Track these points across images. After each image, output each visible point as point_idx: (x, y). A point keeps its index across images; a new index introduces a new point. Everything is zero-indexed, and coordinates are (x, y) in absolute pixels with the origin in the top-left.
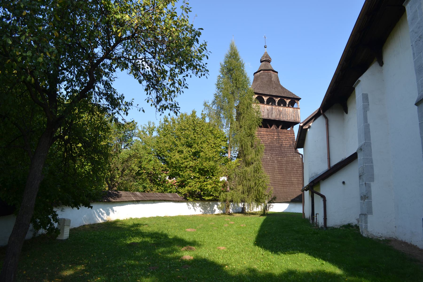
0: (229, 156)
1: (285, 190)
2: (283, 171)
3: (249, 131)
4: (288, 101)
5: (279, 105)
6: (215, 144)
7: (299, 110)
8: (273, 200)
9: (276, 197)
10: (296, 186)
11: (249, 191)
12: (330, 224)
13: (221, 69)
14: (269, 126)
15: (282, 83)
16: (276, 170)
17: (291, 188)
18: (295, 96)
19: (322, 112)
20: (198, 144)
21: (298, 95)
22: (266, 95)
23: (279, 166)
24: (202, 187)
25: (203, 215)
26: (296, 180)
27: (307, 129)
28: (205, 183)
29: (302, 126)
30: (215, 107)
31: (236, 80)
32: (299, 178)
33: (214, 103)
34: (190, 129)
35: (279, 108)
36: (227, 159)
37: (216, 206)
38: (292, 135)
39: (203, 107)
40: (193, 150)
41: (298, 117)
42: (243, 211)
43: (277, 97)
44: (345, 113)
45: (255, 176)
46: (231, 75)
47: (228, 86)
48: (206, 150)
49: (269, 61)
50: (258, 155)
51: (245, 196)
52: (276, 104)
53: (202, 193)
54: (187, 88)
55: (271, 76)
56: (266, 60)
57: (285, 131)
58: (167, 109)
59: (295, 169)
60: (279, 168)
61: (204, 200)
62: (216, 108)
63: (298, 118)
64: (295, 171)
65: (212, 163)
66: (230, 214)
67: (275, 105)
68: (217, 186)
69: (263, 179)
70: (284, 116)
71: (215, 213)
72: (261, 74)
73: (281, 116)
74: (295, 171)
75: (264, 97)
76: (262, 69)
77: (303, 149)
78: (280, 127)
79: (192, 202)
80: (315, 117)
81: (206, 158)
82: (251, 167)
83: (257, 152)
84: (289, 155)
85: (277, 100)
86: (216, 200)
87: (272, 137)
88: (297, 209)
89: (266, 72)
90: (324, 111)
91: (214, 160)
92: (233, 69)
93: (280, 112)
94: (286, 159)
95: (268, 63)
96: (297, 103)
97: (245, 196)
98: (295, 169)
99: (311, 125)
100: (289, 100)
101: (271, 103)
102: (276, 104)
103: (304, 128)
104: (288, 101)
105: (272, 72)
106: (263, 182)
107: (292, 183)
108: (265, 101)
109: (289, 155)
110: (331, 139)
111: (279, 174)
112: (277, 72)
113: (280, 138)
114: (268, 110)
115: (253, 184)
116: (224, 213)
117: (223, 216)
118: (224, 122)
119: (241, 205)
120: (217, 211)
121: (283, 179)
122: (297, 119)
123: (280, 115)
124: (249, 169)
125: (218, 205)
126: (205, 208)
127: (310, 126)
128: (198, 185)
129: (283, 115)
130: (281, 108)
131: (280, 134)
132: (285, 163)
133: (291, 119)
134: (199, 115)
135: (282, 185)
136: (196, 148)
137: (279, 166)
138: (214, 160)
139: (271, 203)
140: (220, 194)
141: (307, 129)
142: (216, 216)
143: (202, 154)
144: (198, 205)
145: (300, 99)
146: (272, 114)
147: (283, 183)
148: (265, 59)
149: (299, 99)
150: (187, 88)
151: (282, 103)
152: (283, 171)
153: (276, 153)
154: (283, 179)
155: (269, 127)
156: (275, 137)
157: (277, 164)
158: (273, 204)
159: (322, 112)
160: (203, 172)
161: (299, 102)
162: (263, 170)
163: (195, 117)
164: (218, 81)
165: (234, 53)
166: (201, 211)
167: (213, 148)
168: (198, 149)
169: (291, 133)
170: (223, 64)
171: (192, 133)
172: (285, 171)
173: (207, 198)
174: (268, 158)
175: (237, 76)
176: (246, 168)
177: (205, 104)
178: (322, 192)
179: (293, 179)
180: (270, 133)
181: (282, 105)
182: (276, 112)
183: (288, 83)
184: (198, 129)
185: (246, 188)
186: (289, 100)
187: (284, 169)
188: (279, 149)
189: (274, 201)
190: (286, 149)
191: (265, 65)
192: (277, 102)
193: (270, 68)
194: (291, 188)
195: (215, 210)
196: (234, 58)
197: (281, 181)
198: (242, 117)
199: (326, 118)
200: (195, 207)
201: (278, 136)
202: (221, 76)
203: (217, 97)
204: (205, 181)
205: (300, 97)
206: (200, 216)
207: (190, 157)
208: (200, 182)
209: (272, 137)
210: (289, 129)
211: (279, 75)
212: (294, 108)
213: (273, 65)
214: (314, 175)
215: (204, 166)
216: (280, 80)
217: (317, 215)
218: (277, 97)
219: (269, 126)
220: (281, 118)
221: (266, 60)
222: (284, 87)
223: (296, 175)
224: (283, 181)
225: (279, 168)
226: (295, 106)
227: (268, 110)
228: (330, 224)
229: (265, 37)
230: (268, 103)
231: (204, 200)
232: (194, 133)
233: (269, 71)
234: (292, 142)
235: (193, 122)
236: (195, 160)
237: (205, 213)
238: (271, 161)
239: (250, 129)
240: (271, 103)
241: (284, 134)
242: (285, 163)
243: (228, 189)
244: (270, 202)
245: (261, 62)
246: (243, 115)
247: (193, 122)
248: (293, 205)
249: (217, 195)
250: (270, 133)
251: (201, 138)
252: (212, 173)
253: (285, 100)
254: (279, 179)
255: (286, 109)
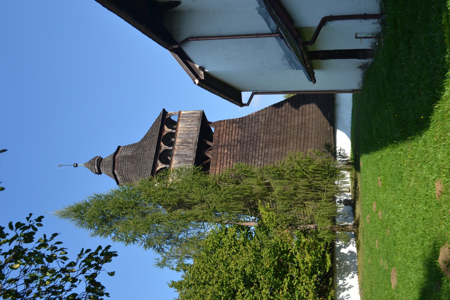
0: (253, 224)
1: (313, 136)
2: (282, 139)
3: (210, 187)
4: (167, 130)
5: (172, 144)
6: (230, 247)
7: (182, 112)
8: (331, 148)
9: (326, 145)
10: (307, 117)
11: (317, 189)
12: (374, 8)
13: (101, 235)
14: (207, 161)
15: (137, 139)
16: (281, 150)
17: (310, 126)
18: (158, 118)
19: (176, 46)
20: (230, 279)
21: (156, 114)
22: (155, 165)
23: (274, 145)
24: (309, 273)
25: (360, 272)
26: (296, 118)
27: (205, 73)
28: (301, 265)
29: (200, 80)
30: (167, 248)
31: (122, 208)
32: (293, 114)
33: (160, 250)
34: (202, 292)
35: (177, 144)
36: (259, 226)
37: (343, 250)
38: (222, 123)
39: (166, 268)
40: (241, 287)
41: (193, 113)
42: (351, 204)
43: (158, 147)
44: (180, 6)
45: (288, 177)
46: (113, 217)
47: (131, 222)
48: (241, 262)
49: (100, 160)
50: (253, 174)
51: (324, 196)
52: (171, 148)
53: (319, 272)
54: (40, 219)
55: (125, 157)
56: (97, 165)
57: (215, 136)
58: (97, 279)
59: (279, 120)
60: (278, 145)
61: (332, 269)
62: (170, 246)
63: (195, 113)
64: (283, 120)
65: (265, 252)
66: (357, 225)
67: (171, 150)
68: (307, 244)
69: (296, 164)
70: (192, 136)
71: (356, 252)
72: (119, 174)
73: (191, 140)
74: (283, 120)
75: (158, 169)
76: (111, 171)
77: (242, 93)
78: (209, 143)
79: (335, 292)
80: (185, 59)
81: (256, 262)
82: (273, 183)
83: (249, 174)
84: (256, 129)
85: (164, 147)
86: (332, 249)
87: (225, 156)
88: (345, 105)
89: (116, 165)
90: (176, 43)
91: (259, 248)
92: (103, 214)
93: (185, 142)
94: (262, 135)
95: (103, 161)
96: (171, 115)
97: (324, 196)
98: (279, 120)
99: (197, 66)
100: (166, 127)
101: (169, 158)
102: (171, 148)
103: (203, 78)
104: (167, 130)
105: (118, 155)
106: (299, 164)
107: (302, 124)
108: (164, 166)
109: (256, 129)
110: (222, 33)
111: (288, 146)
112: (119, 147)
113: (227, 143)
114: (180, 162)
115: (303, 182)
116: (356, 236)
117: (360, 237)
118: (193, 232)
119: (341, 208)
120: (352, 248)
121: (295, 140)
122: (196, 115)
123: (189, 143)
124: (277, 188)
125: (341, 247)
126: (347, 270)
127: (200, 67)
128: (305, 278)
129: (189, 138)
130: (178, 140)
131: (220, 144)
132: (268, 135)
133: (196, 125)
134: (178, 276)
135: (306, 141)
136: (238, 283)
137: (274, 145)
138: (259, 248)
139: (336, 153)
140: (321, 240)
141: (205, 73)
142: (360, 251)
143: (248, 270)
144: (341, 282)
145: (164, 110)
146: (186, 155)
147: (302, 138)
148: (96, 167)
149: (164, 112)
150: (40, 219)
151: (169, 140)
152: (282, 139)
153: (251, 149)
154: (295, 140)
155: (209, 160)
156: (226, 151)
157: (270, 149)
158: (338, 149)
159: (176, 46)
160: (281, 270)
161: (169, 112)
162: (278, 164)
163: (181, 283)
164: (122, 240)
165: (76, 211)
166: (353, 277)
167: (238, 251)
168: (239, 277)
169: (220, 126)
170: (93, 231)
171: (211, 288)
172: (282, 136)
173: (329, 263)
174: (259, 163)
175: (114, 206)
176: (275, 193)
177: (161, 265)
178: (314, 23)
179: (296, 124)
180: (219, 159)
181: (173, 139)
182: (183, 149)
183: (137, 129)
184: (204, 277)
185: (311, 195)
186: (166, 127)
187: (278, 137)
188: (245, 145)
189: (333, 147)
190: (246, 134)
191: (105, 167)
192: (167, 148)
193: (111, 159)
194: (310, 126)
195: (350, 252)
196: (85, 212)
197: (298, 141)
198: (187, 200)
199: (187, 40)
200: (346, 287)
201: (223, 146)
202: (113, 235)
203: (149, 244)
204: (298, 267)
205: (161, 111)
206: (363, 277)
207: (253, 294)
208: (299, 275)
209: (225, 156)
210: (213, 129)
211: (122, 145)
212: (179, 120)
213: (106, 153)
214: (286, 61)
215: (270, 266)
216: (132, 143)
217: (358, 36)
218: (158, 147)
219: (207, 161)
220: (194, 140)
221: (97, 165)
222: (143, 137)
223: (289, 118)
224: (299, 139)
225: (278, 145)
226: (175, 118)
227: (180, 162)
228: (374, 8)
229: (61, 165)
230: (168, 162)
231: (332, 269)
232: (210, 285)
233: (116, 160)
234: (234, 125)
235: (190, 286)
236: (258, 283)
237: (356, 270)
238: (265, 159)
239: (207, 184)
240: (169, 158)
241: (221, 137)
242: (268, 135)
243: (312, 226)
244: (334, 154)
245: (100, 173)
246: (183, 197)
247: (190, 286)
248: (339, 123)
249: (322, 244)
250: (219, 159)
251: (220, 272)
252: (283, 253)
253: (164, 134)
254: (295, 145)
255: (179, 132)
